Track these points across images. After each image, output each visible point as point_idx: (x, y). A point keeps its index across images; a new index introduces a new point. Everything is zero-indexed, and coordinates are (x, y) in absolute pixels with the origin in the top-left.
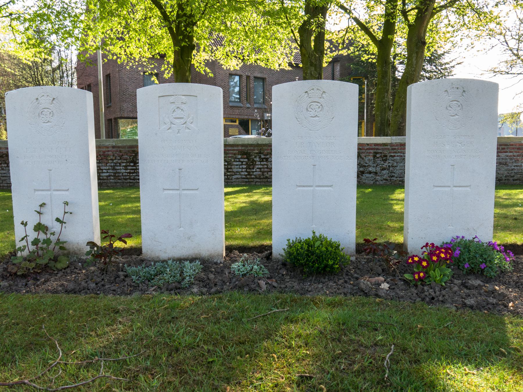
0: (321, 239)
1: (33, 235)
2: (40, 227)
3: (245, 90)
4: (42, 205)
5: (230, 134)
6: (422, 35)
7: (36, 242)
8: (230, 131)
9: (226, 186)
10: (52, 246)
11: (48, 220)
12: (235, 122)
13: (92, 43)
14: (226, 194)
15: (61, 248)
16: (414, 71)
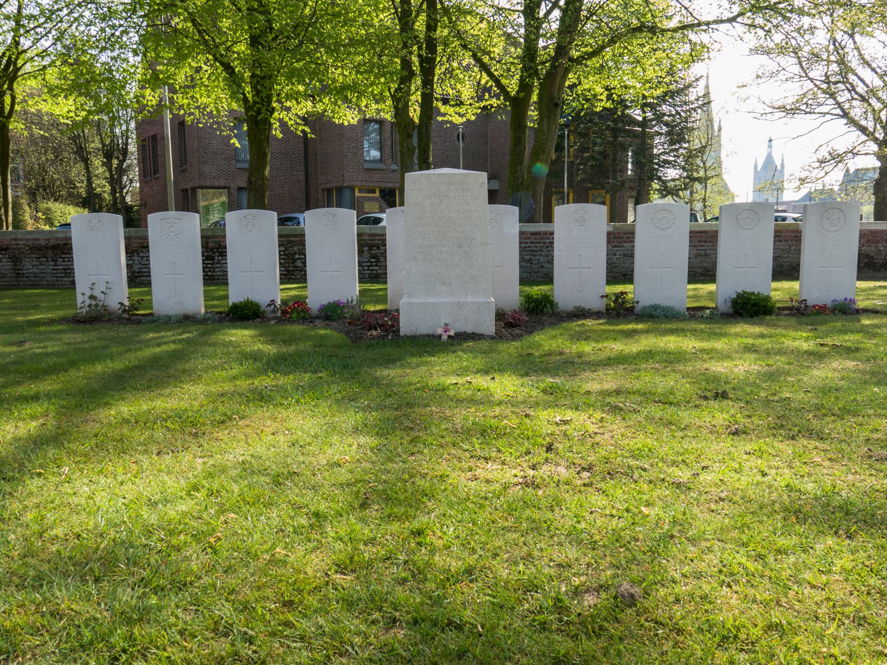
0: (252, 303)
1: (88, 302)
2: (92, 297)
3: (389, 143)
4: (93, 284)
5: (366, 210)
6: (556, 94)
7: (90, 306)
8: (365, 206)
9: (282, 283)
10: (99, 308)
11: (97, 293)
12: (374, 192)
13: (150, 98)
14: (281, 290)
15: (105, 310)
16: (546, 139)
